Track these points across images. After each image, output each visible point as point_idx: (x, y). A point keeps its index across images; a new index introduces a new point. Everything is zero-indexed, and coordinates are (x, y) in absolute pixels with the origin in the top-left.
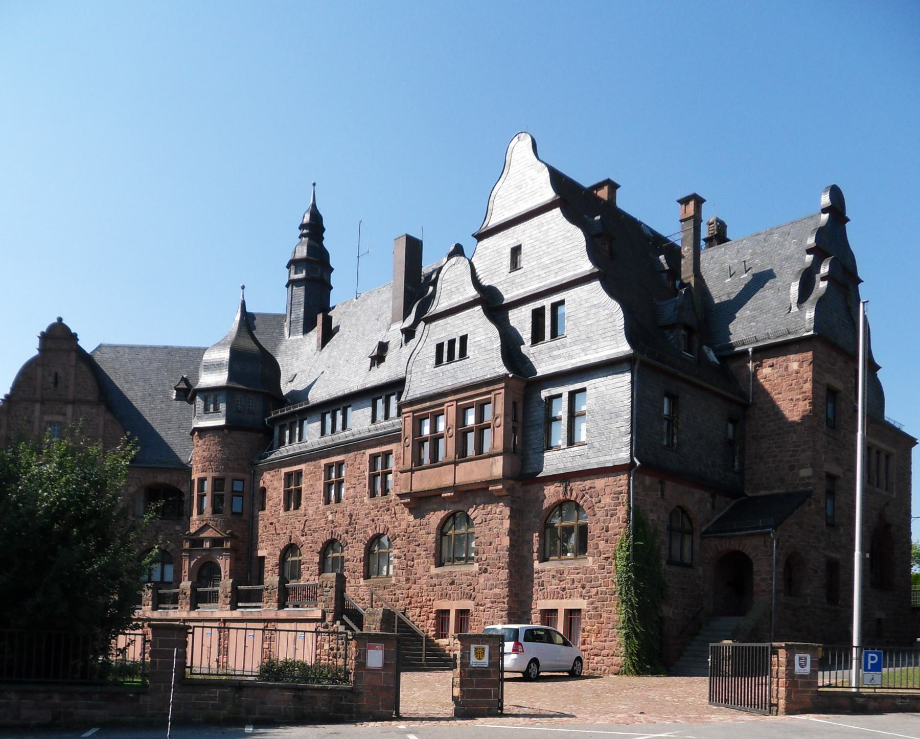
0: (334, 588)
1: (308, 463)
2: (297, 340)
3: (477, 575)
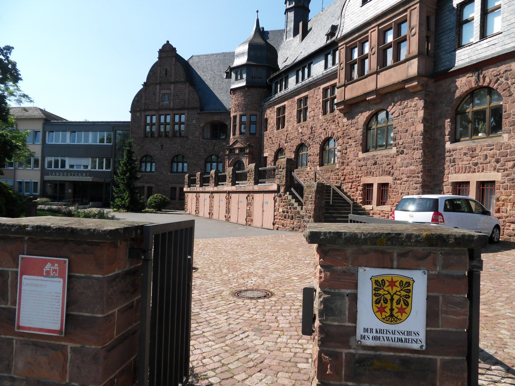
0: (285, 169)
1: (288, 100)
2: (290, 41)
3: (395, 156)
